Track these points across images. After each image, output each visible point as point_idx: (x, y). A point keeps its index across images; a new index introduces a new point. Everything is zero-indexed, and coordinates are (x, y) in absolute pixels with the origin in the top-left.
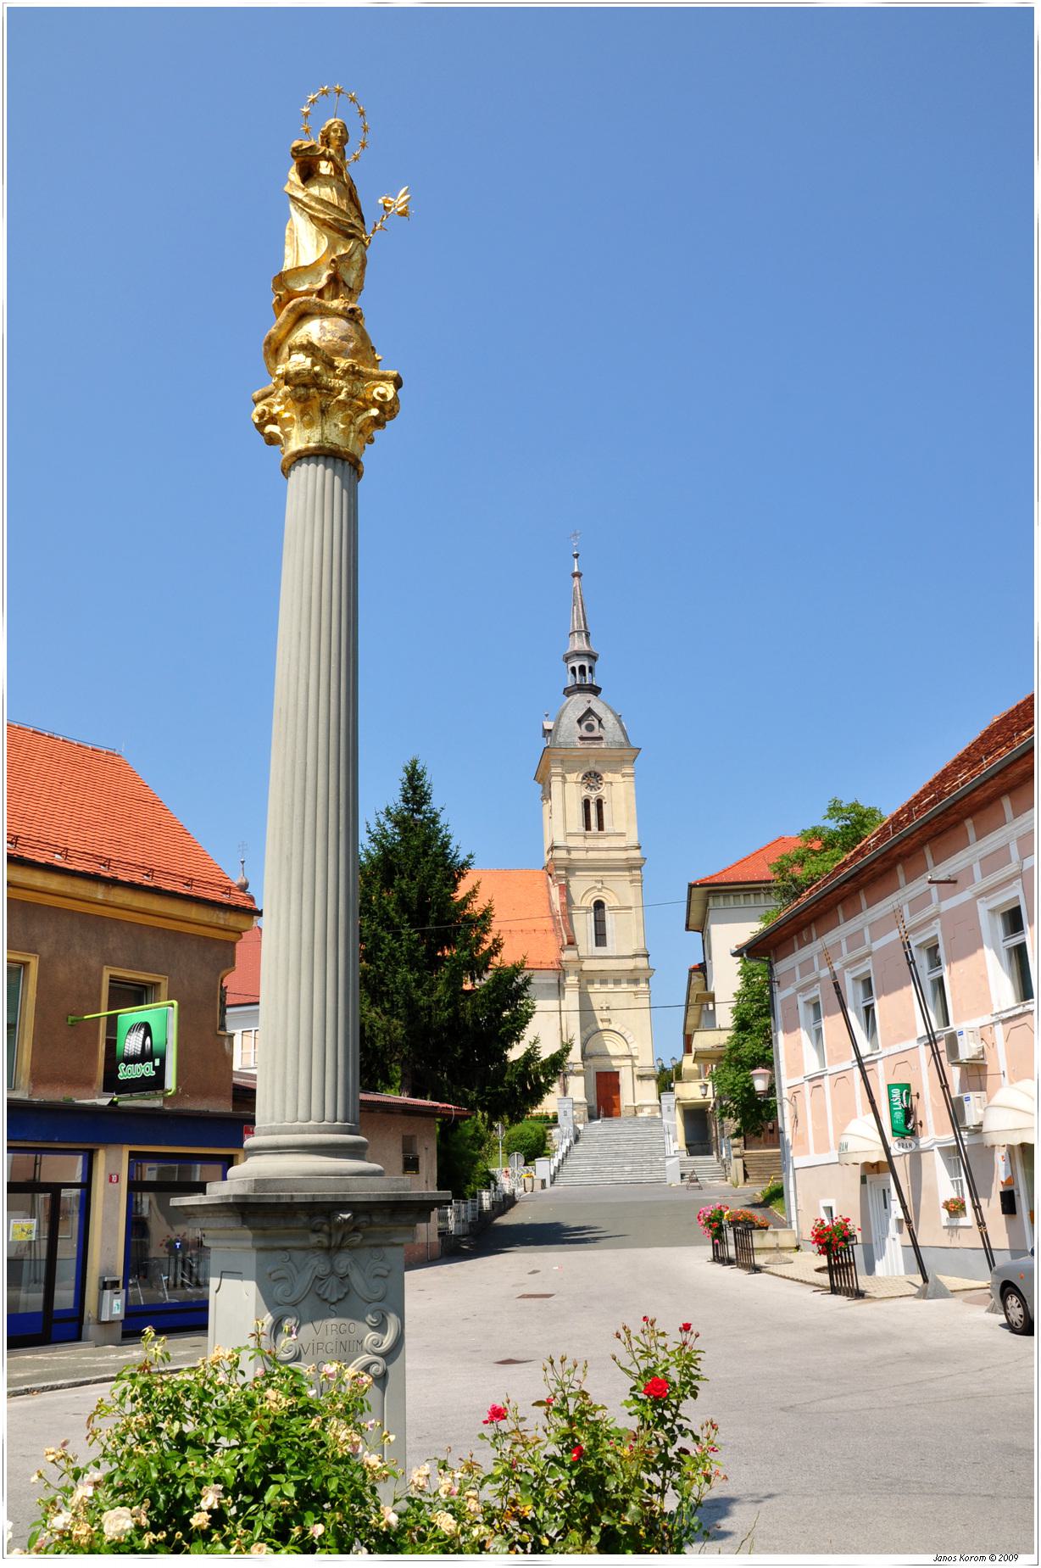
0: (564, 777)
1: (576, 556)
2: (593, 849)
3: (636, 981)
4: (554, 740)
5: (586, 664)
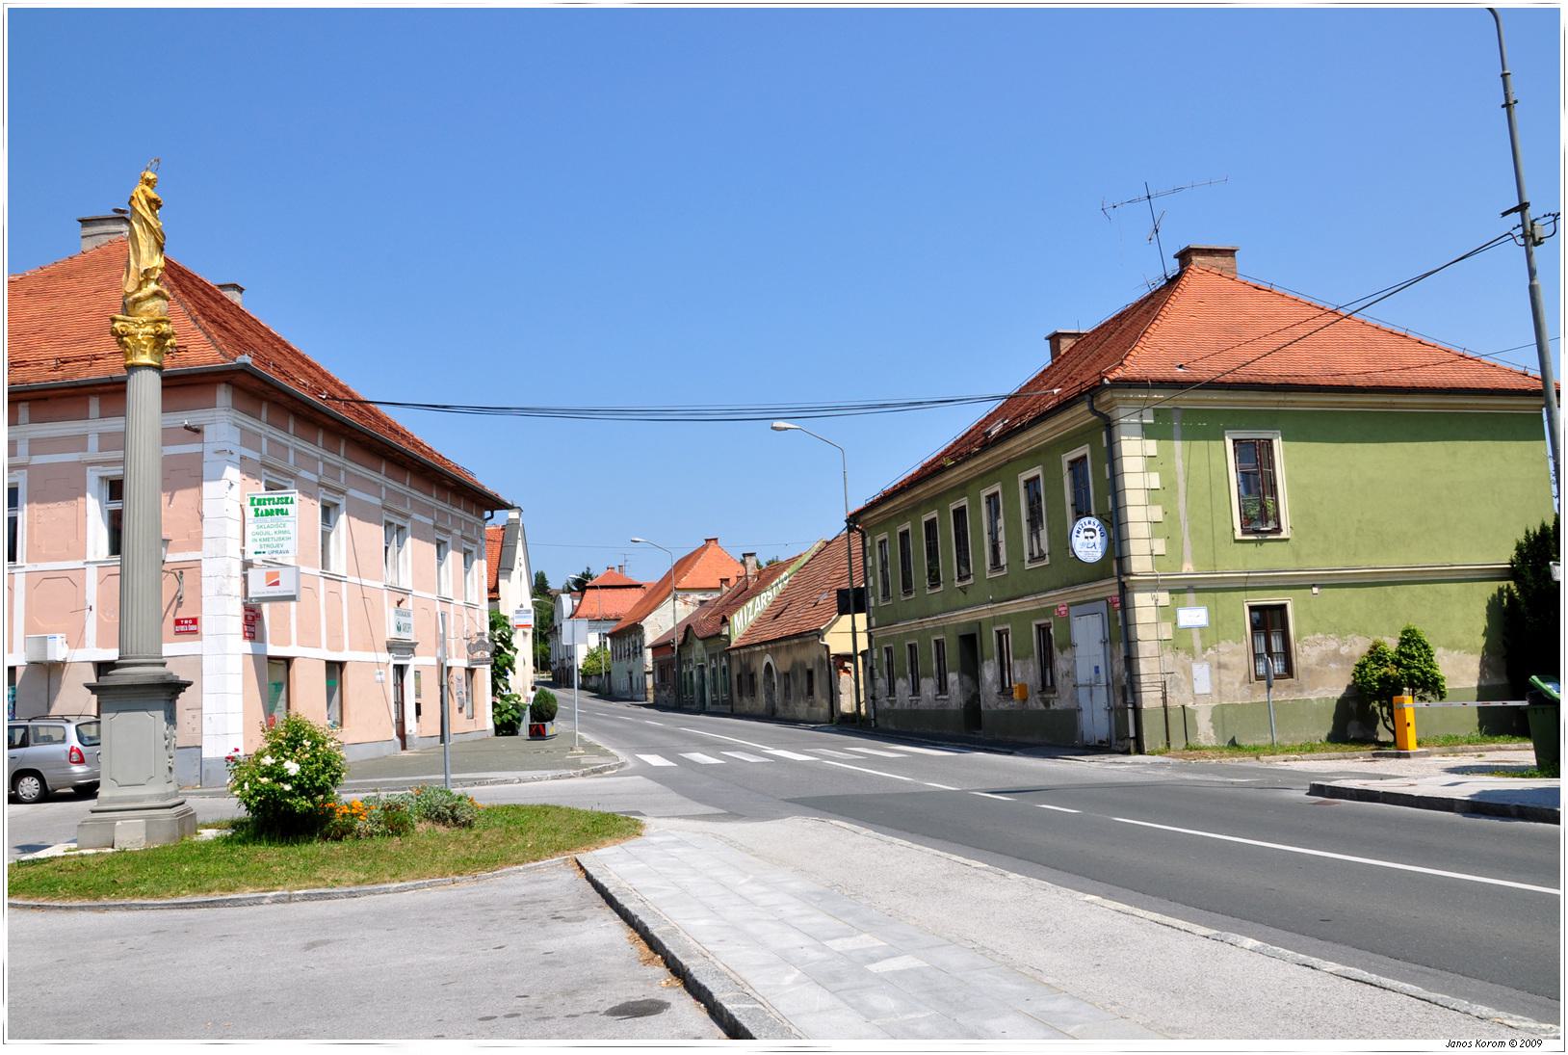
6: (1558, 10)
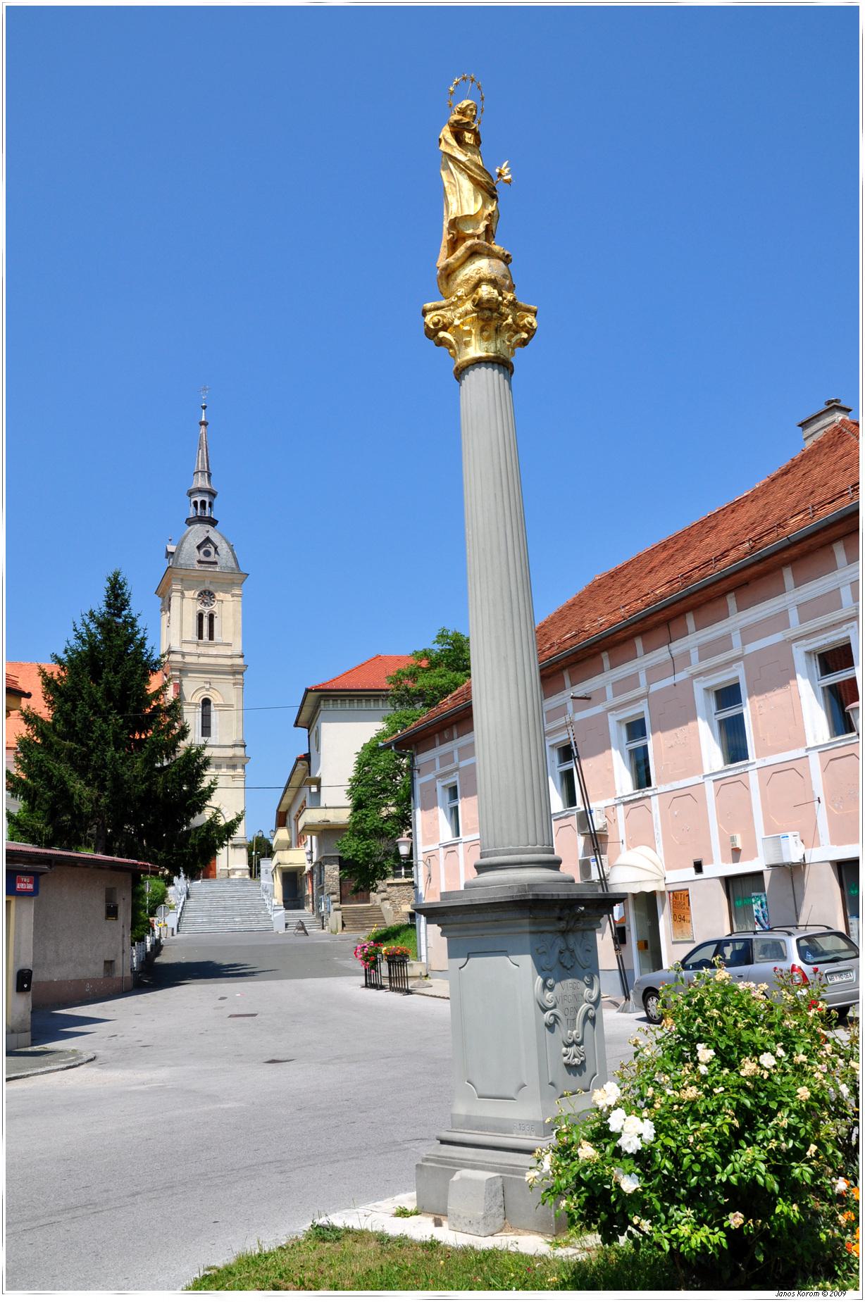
0: (182, 593)
1: (204, 408)
2: (204, 655)
3: (234, 767)
4: (176, 561)
5: (207, 499)
6: (858, 7)
